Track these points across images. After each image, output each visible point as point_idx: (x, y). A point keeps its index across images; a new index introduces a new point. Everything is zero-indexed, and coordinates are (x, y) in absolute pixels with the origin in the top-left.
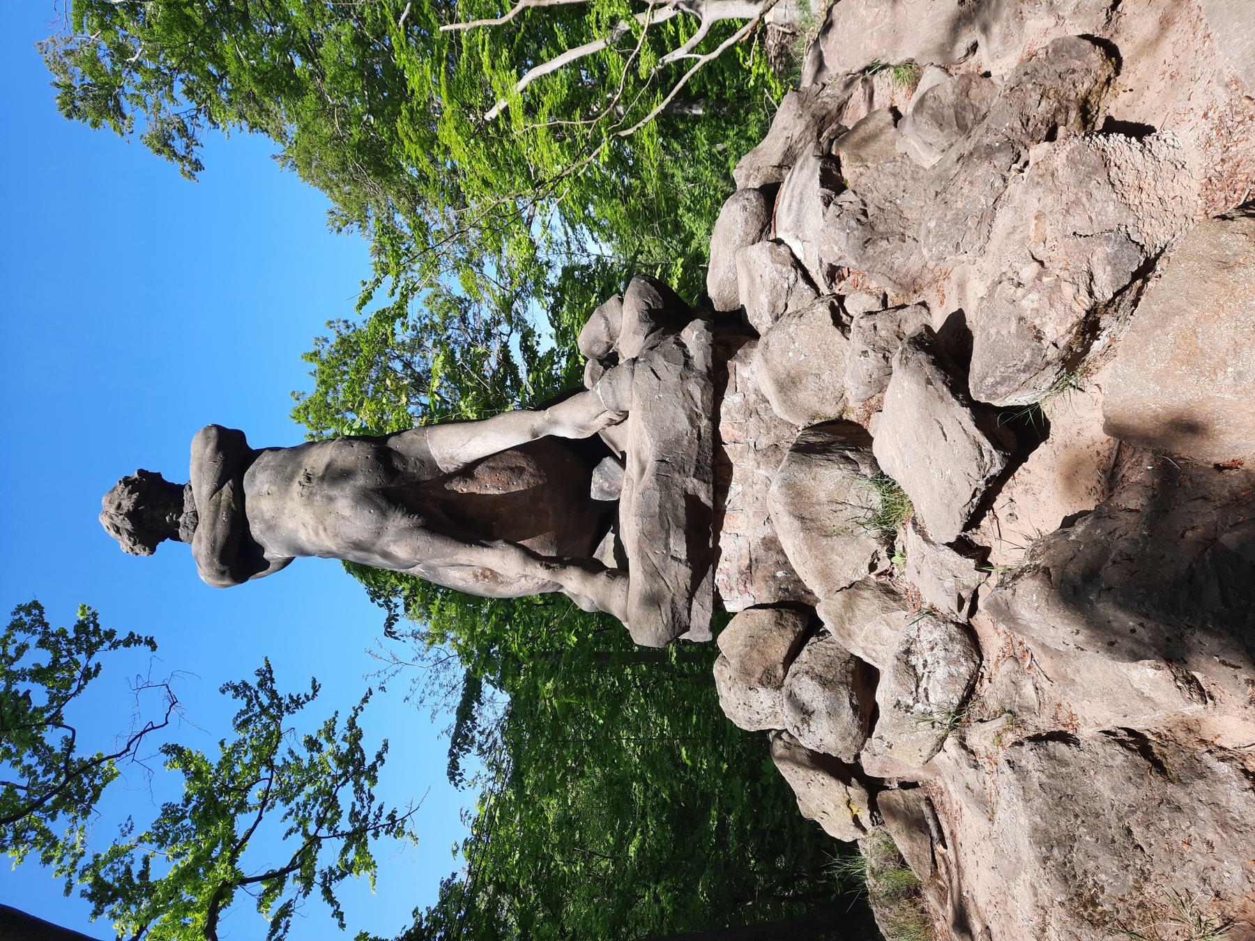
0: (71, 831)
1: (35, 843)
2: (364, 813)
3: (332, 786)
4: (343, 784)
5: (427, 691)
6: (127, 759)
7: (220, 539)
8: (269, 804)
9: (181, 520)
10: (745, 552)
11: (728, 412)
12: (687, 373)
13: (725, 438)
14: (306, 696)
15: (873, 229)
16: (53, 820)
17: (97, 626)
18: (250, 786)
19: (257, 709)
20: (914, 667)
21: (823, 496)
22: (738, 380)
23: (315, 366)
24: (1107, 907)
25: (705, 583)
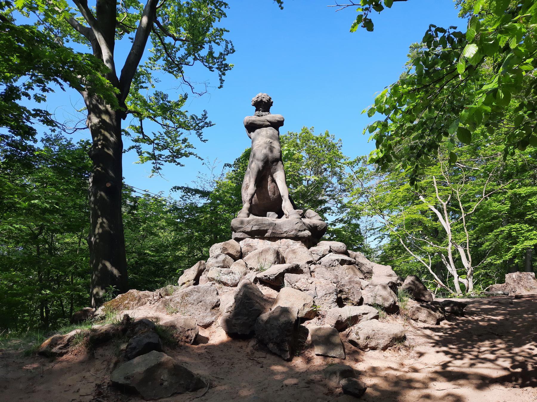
0: (159, 66)
1: (156, 55)
2: (161, 159)
3: (170, 148)
4: (170, 151)
5: (202, 179)
6: (182, 81)
7: (256, 122)
8: (164, 127)
10: (254, 245)
11: (288, 241)
14: (202, 138)
16: (163, 60)
17: (227, 70)
18: (172, 121)
19: (198, 122)
21: (267, 257)
23: (324, 135)
24: (186, 298)
25: (246, 235)
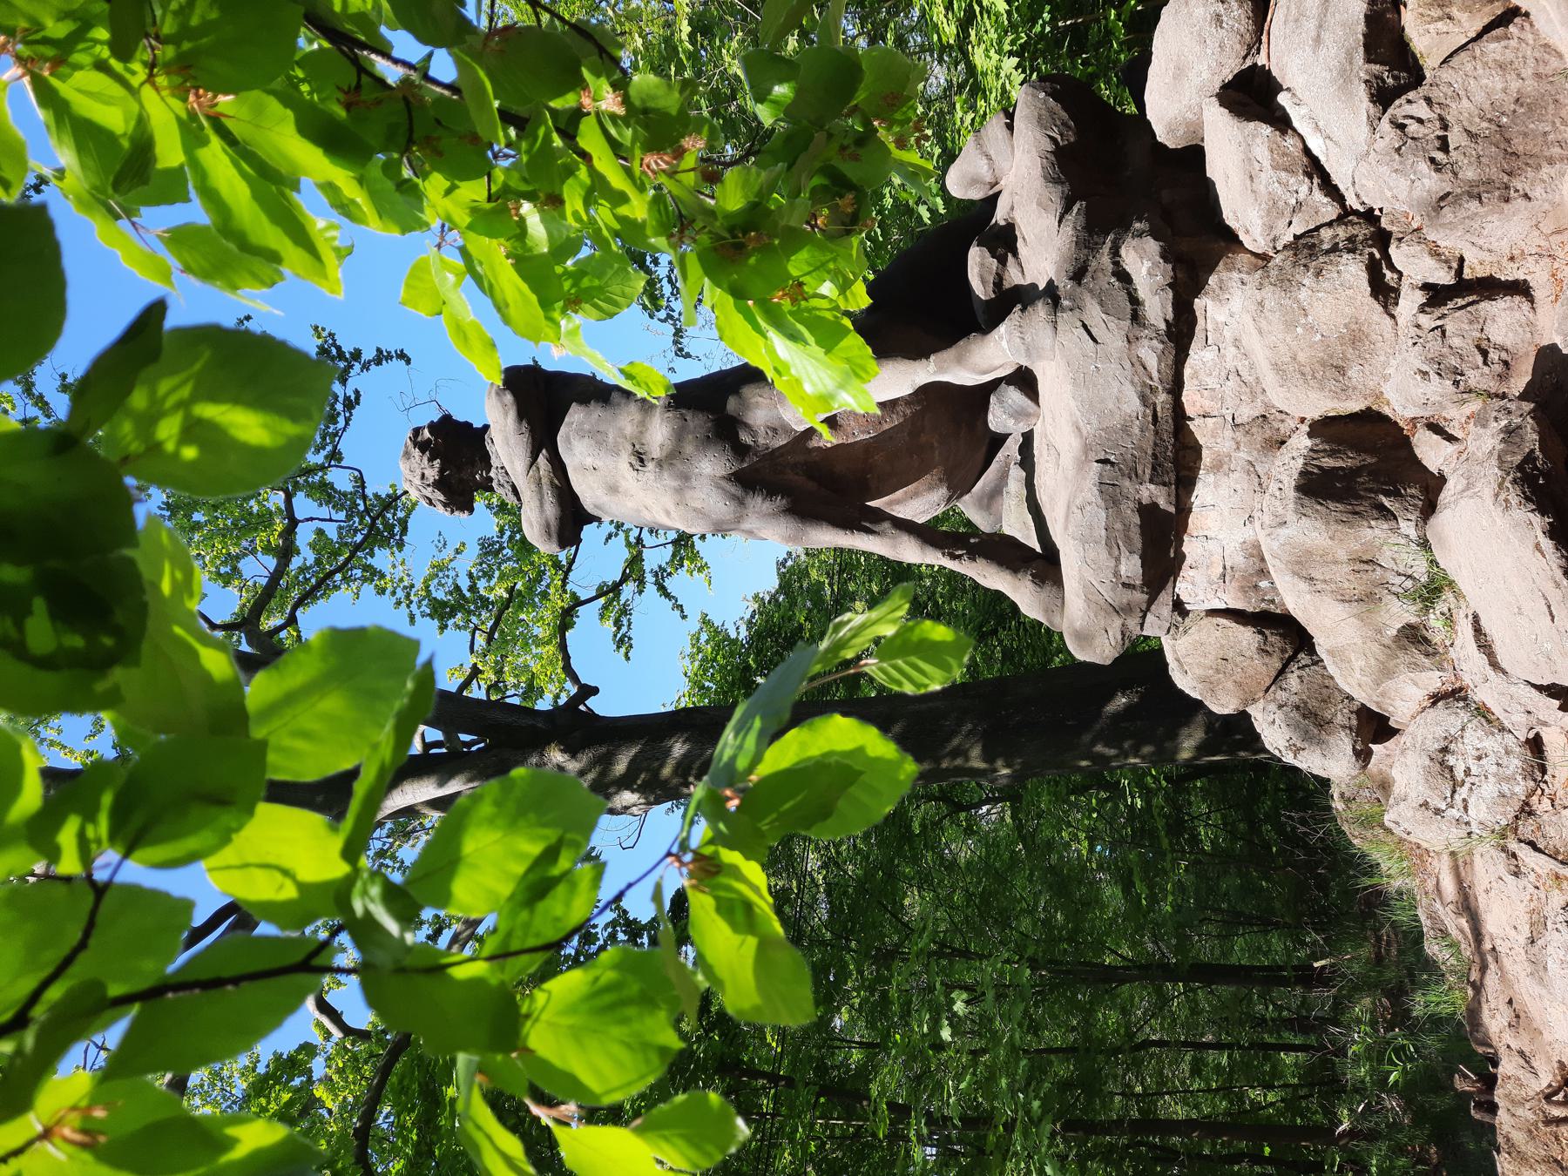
0: (394, 566)
1: (364, 580)
7: (554, 523)
9: (492, 474)
10: (1217, 559)
11: (1195, 375)
12: (1137, 331)
13: (1190, 410)
15: (1455, 174)
17: (339, 348)
20: (1451, 769)
22: (1209, 327)
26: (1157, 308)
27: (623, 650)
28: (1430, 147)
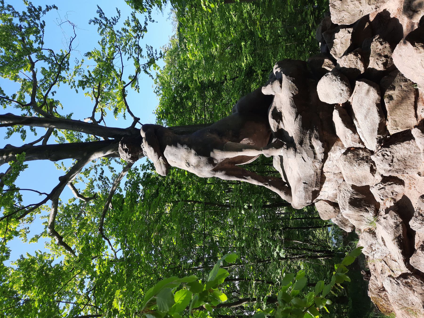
11: (327, 165)
12: (315, 160)
15: (394, 167)
17: (34, 7)
19: (103, 27)
20: (372, 248)
22: (331, 157)
26: (320, 156)
27: (137, 90)
28: (389, 162)
